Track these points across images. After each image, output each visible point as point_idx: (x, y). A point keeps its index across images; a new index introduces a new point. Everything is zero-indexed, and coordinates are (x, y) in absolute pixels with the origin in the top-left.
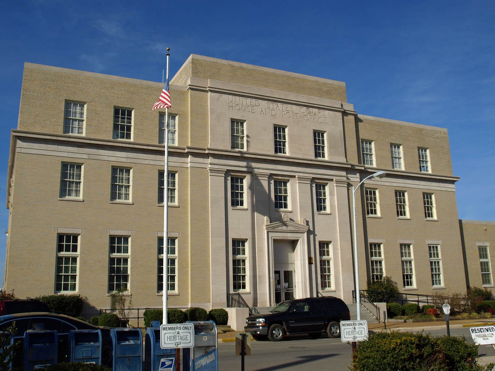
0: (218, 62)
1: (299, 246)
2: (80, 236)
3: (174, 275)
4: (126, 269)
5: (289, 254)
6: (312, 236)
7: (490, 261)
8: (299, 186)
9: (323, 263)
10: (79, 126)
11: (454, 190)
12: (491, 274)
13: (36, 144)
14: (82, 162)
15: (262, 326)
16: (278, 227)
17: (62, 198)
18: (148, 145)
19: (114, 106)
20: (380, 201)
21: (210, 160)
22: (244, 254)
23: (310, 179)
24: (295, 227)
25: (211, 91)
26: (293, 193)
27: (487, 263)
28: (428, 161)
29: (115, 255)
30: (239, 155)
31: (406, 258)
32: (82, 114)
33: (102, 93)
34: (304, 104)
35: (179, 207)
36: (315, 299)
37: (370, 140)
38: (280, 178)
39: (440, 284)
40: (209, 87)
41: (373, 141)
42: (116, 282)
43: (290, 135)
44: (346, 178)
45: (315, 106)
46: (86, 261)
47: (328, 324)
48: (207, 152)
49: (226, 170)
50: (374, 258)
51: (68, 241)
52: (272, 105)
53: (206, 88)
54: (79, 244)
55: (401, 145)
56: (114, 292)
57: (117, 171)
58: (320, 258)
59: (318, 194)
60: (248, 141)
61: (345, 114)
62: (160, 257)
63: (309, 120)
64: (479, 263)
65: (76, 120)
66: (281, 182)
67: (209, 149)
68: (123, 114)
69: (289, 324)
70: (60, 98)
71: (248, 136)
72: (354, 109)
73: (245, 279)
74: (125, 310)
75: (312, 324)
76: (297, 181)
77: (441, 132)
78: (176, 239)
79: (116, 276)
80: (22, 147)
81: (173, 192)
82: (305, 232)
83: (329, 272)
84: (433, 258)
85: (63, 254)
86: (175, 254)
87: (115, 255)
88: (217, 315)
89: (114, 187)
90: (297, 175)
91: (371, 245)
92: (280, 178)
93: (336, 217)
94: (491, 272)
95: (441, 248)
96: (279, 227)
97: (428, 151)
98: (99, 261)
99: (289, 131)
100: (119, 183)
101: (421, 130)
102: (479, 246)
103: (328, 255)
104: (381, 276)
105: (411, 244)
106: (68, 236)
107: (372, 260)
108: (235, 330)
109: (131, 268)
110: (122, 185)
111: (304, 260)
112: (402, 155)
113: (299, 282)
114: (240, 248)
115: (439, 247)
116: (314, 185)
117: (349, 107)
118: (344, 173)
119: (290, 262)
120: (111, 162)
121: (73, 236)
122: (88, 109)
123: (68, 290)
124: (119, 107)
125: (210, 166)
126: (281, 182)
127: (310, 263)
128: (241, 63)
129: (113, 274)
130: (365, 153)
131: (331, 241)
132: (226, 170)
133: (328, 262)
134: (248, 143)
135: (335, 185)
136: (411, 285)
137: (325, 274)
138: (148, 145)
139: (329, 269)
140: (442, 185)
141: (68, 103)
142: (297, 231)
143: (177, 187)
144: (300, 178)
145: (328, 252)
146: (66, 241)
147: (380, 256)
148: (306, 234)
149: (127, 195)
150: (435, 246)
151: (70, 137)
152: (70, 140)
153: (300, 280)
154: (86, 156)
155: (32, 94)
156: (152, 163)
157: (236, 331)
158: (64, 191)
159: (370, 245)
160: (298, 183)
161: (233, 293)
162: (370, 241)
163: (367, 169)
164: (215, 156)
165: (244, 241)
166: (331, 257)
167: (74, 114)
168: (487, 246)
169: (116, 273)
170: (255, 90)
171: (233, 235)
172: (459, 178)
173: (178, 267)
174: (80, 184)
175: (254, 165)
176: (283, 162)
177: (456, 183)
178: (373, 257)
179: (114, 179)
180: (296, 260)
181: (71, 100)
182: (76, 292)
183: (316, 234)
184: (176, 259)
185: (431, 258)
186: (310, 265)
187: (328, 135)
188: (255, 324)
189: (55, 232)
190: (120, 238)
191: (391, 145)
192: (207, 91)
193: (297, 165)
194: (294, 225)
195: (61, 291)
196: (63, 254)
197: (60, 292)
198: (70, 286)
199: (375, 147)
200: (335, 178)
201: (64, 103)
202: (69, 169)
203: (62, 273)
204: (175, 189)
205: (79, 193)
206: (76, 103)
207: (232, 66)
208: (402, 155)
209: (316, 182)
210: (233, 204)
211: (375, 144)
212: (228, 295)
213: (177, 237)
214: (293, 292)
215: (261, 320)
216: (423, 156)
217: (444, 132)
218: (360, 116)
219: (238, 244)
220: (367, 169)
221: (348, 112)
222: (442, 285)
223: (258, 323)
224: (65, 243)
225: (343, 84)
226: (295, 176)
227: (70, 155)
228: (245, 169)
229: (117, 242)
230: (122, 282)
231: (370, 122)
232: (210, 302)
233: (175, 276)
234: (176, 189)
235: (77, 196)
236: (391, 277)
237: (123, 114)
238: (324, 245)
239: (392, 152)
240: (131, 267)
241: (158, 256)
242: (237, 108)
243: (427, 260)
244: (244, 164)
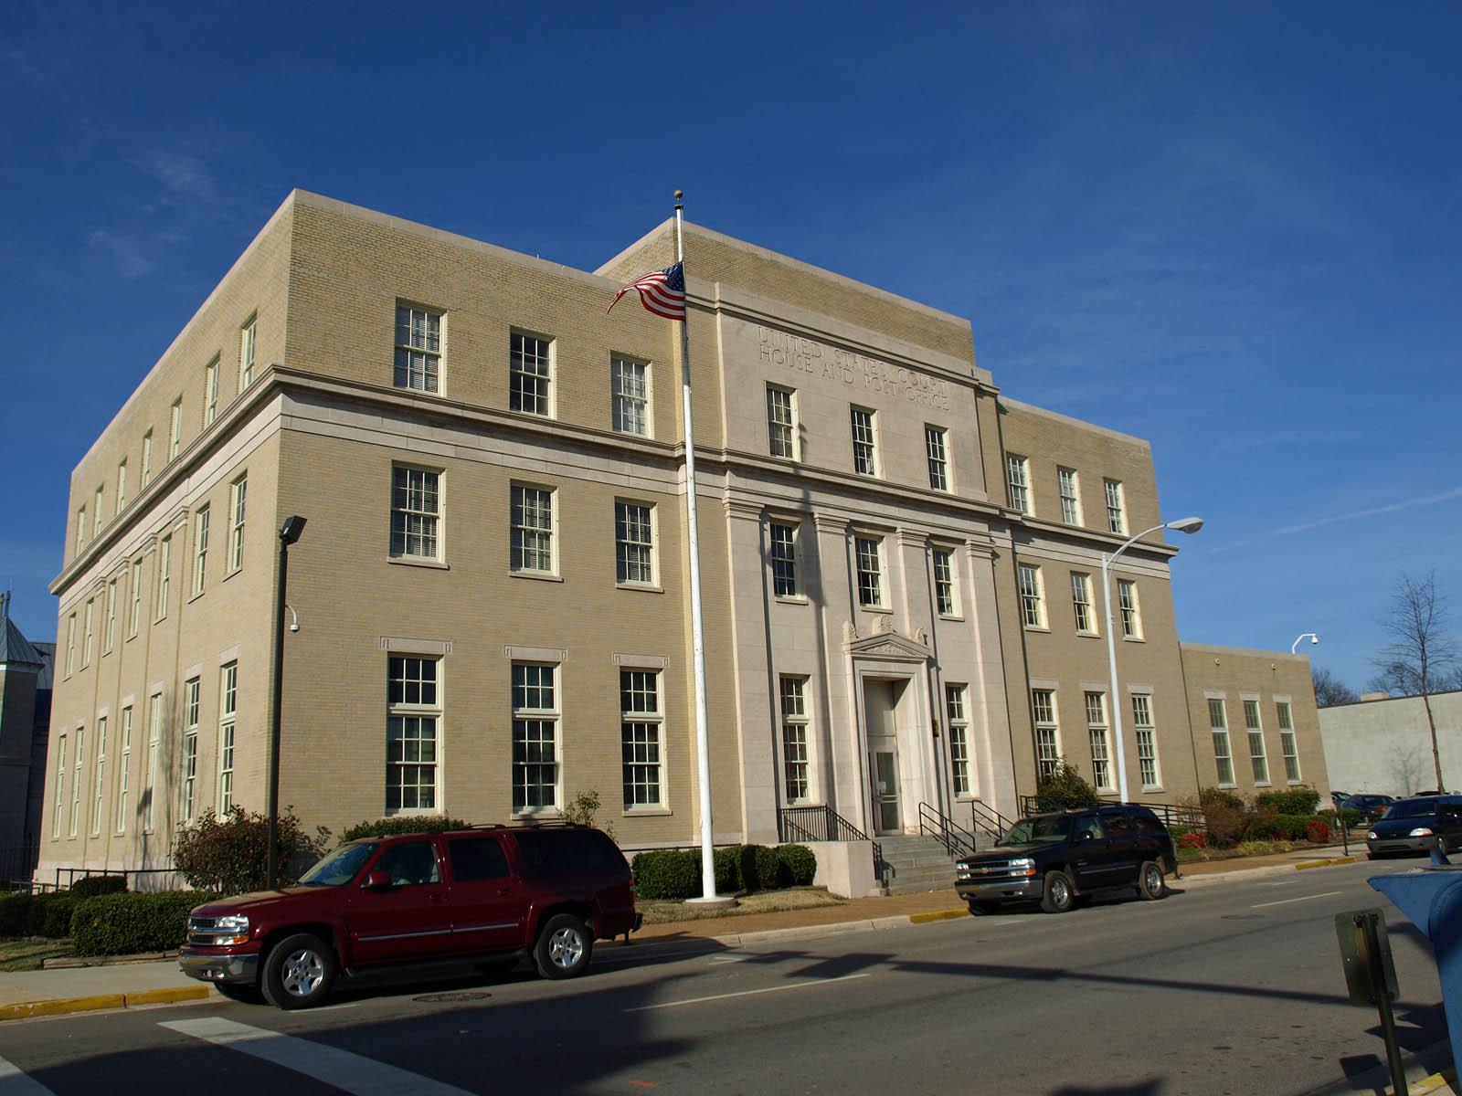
0: (726, 243)
1: (910, 690)
2: (442, 660)
3: (657, 763)
4: (550, 749)
5: (885, 712)
6: (933, 670)
7: (1262, 732)
8: (732, 525)
9: (953, 731)
10: (426, 369)
11: (1167, 576)
12: (1297, 759)
13: (330, 410)
14: (441, 466)
15: (1031, 878)
17: (515, 571)
18: (463, 407)
19: (512, 327)
20: (1046, 595)
21: (728, 479)
22: (655, 709)
23: (844, 522)
24: (904, 648)
25: (724, 311)
26: (893, 568)
27: (1224, 734)
28: (1026, 488)
29: (525, 712)
30: (790, 470)
31: (1043, 723)
32: (434, 340)
33: (483, 289)
35: (563, 582)
36: (467, 847)
37: (642, 359)
38: (866, 531)
39: (655, 798)
40: (720, 301)
41: (1026, 458)
42: (528, 783)
43: (882, 431)
44: (988, 538)
46: (460, 729)
47: (1140, 866)
48: (724, 458)
49: (763, 506)
51: (413, 673)
52: (848, 359)
53: (714, 303)
54: (440, 682)
55: (1075, 470)
56: (527, 809)
57: (526, 494)
58: (784, 720)
59: (862, 562)
60: (802, 440)
61: (979, 391)
62: (393, 712)
63: (916, 400)
64: (1211, 736)
65: (420, 354)
66: (866, 541)
67: (729, 453)
68: (530, 349)
69: (1079, 870)
70: (384, 293)
71: (801, 427)
72: (994, 381)
73: (805, 774)
74: (60, 883)
75: (449, 931)
76: (900, 541)
77: (1139, 447)
78: (439, 659)
79: (528, 766)
81: (431, 525)
82: (921, 662)
83: (804, 756)
84: (1140, 725)
85: (403, 707)
86: (434, 703)
87: (525, 712)
88: (795, 862)
89: (397, 518)
90: (900, 526)
91: (1035, 691)
92: (866, 531)
93: (973, 628)
94: (1297, 755)
95: (1153, 702)
97: (1026, 463)
98: (491, 729)
99: (880, 421)
100: (410, 508)
101: (1106, 441)
102: (1210, 699)
103: (801, 711)
104: (1054, 764)
105: (1102, 693)
106: (413, 660)
107: (626, 719)
108: (846, 896)
109: (565, 747)
110: (532, 531)
111: (923, 727)
112: (1076, 493)
113: (912, 780)
114: (538, 689)
115: (1149, 699)
116: (767, 526)
117: (985, 378)
118: (984, 528)
119: (887, 732)
120: (506, 469)
121: (423, 661)
122: (450, 329)
123: (417, 806)
124: (522, 330)
125: (728, 494)
126: (866, 541)
127: (935, 735)
128: (773, 253)
129: (522, 763)
130: (408, 350)
131: (967, 684)
132: (763, 506)
133: (801, 729)
134: (804, 444)
135: (969, 553)
136: (802, 796)
137: (793, 762)
138: (463, 407)
139: (803, 748)
140: (627, 467)
141: (403, 307)
142: (909, 657)
143: (442, 511)
144: (906, 534)
145: (800, 702)
146: (408, 675)
147: (653, 707)
148: (924, 665)
149: (431, 543)
150: (1142, 697)
151: (415, 397)
152: (415, 406)
153: (916, 774)
154: (450, 451)
155: (316, 273)
156: (600, 477)
157: (850, 897)
158: (398, 544)
159: (781, 680)
160: (903, 544)
161: (788, 806)
162: (1034, 684)
164: (740, 470)
165: (801, 680)
166: (807, 717)
167: (627, 390)
168: (1221, 700)
169: (637, 761)
170: (902, 348)
171: (783, 666)
172: (1177, 550)
173: (667, 743)
174: (434, 524)
175: (816, 496)
176: (713, 465)
177: (1170, 560)
178: (628, 712)
179: (398, 498)
180: (901, 728)
181: (409, 301)
182: (439, 809)
184: (438, 716)
185: (1137, 725)
187: (952, 437)
188: (211, 938)
189: (382, 649)
190: (520, 666)
191: (616, 358)
192: (713, 311)
193: (384, 410)
195: (525, 807)
196: (403, 707)
197: (397, 812)
198: (421, 795)
199: (1032, 473)
200: (969, 539)
201: (394, 307)
202: (411, 479)
203: (401, 760)
204: (651, 547)
205: (434, 546)
206: (421, 310)
207: (756, 258)
208: (1076, 493)
209: (772, 519)
210: (779, 590)
211: (1031, 465)
212: (779, 811)
213: (662, 669)
214: (896, 803)
215: (1025, 862)
216: (1016, 475)
217: (1144, 448)
218: (1002, 400)
219: (791, 684)
221: (985, 388)
222: (1159, 783)
223: (222, 935)
224: (526, 686)
225: (966, 324)
226: (896, 528)
227: (413, 445)
228: (794, 506)
229: (530, 679)
230: (543, 783)
231: (1022, 416)
232: (741, 831)
233: (434, 766)
234: (441, 517)
235: (426, 554)
236: (1076, 766)
237: (530, 349)
238: (954, 690)
239: (615, 382)
240: (563, 745)
241: (388, 707)
242: (777, 356)
243: (611, 717)
244: (797, 493)
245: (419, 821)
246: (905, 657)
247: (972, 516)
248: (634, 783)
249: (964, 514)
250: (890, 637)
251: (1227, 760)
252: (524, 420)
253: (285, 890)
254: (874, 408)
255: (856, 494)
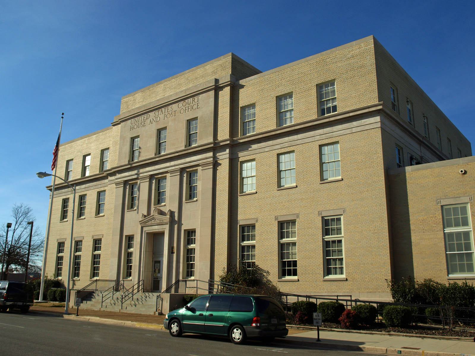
7: (472, 229)
16: (148, 222)
18: (177, 152)
23: (121, 182)
34: (179, 99)
45: (189, 96)
50: (246, 243)
80: (315, 135)
92: (159, 176)
96: (149, 221)
142: (162, 223)
163: (239, 141)
171: (126, 233)
183: (182, 223)
186: (172, 254)
194: (158, 217)
209: (187, 172)
220: (239, 141)
245: (223, 278)
246: (161, 223)
247: (204, 152)
248: (292, 268)
249: (199, 153)
250: (154, 216)
251: (343, 268)
252: (330, 116)
253: (140, 290)
254: (166, 126)
255: (199, 153)
